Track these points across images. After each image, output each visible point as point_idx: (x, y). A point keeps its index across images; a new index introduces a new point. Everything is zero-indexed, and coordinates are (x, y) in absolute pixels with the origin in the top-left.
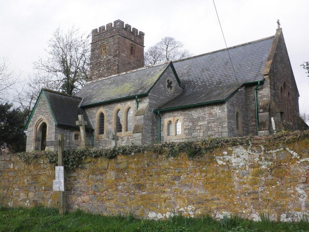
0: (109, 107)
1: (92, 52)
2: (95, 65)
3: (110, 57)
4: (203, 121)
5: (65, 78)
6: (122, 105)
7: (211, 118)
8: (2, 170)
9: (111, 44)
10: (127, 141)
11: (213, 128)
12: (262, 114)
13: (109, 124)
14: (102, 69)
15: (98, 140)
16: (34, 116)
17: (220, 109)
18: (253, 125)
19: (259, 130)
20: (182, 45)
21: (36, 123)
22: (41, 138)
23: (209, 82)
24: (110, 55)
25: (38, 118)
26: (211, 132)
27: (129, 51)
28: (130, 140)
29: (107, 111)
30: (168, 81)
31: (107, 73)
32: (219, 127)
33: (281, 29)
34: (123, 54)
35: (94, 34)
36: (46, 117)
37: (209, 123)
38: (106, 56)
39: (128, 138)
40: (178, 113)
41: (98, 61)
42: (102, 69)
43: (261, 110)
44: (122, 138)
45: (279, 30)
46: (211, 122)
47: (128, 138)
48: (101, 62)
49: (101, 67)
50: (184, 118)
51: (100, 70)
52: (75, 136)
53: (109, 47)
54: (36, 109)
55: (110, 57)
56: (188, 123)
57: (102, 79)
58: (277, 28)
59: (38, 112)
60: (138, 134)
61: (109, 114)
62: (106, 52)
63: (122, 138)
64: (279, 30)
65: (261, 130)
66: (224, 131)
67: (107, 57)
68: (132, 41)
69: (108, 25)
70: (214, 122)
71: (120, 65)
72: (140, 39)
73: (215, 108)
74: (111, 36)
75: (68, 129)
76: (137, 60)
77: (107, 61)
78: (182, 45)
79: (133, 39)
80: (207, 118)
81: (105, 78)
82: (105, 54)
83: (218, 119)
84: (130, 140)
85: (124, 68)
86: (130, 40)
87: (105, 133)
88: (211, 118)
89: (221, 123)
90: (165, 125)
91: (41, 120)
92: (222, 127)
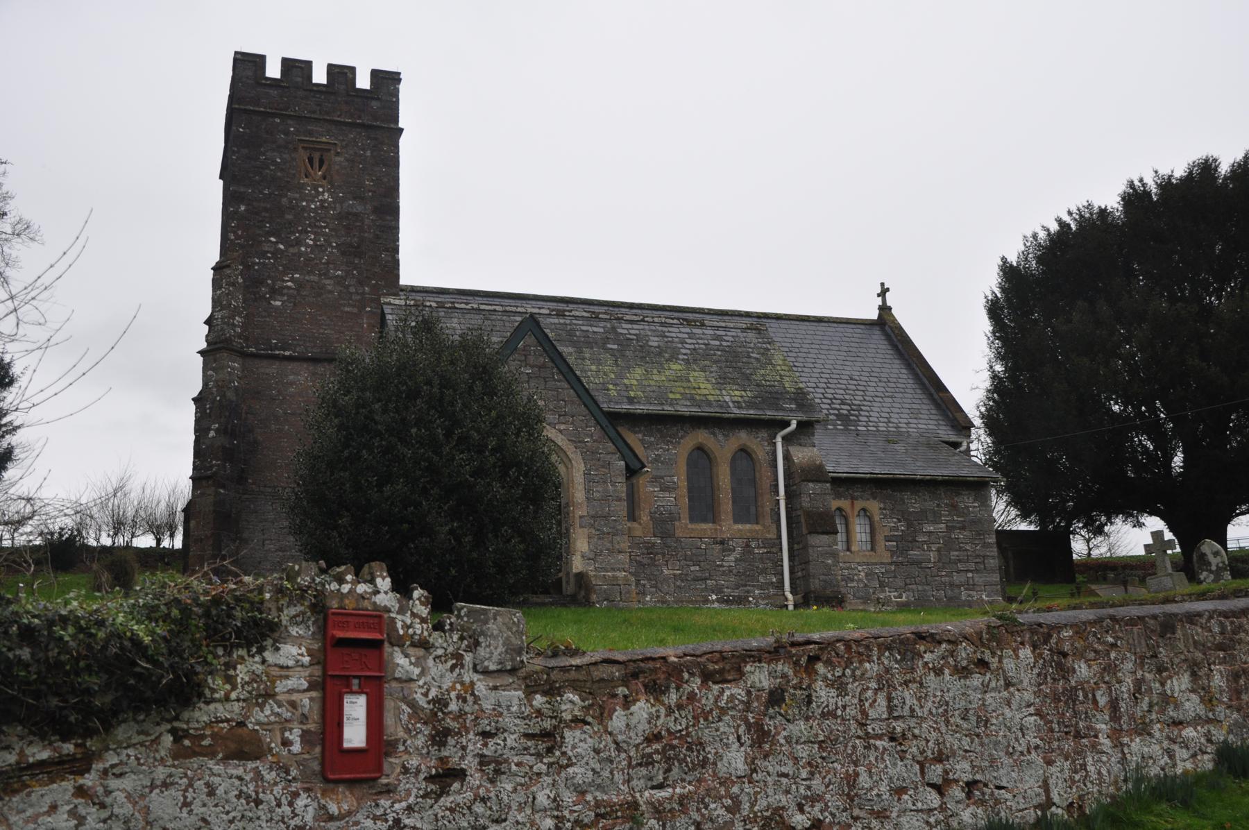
6: (714, 434)
10: (743, 554)
17: (975, 501)
29: (651, 443)
36: (561, 431)
37: (950, 529)
39: (748, 546)
41: (284, 200)
44: (722, 543)
47: (748, 546)
51: (299, 243)
63: (722, 543)
70: (963, 528)
77: (340, 217)
83: (973, 522)
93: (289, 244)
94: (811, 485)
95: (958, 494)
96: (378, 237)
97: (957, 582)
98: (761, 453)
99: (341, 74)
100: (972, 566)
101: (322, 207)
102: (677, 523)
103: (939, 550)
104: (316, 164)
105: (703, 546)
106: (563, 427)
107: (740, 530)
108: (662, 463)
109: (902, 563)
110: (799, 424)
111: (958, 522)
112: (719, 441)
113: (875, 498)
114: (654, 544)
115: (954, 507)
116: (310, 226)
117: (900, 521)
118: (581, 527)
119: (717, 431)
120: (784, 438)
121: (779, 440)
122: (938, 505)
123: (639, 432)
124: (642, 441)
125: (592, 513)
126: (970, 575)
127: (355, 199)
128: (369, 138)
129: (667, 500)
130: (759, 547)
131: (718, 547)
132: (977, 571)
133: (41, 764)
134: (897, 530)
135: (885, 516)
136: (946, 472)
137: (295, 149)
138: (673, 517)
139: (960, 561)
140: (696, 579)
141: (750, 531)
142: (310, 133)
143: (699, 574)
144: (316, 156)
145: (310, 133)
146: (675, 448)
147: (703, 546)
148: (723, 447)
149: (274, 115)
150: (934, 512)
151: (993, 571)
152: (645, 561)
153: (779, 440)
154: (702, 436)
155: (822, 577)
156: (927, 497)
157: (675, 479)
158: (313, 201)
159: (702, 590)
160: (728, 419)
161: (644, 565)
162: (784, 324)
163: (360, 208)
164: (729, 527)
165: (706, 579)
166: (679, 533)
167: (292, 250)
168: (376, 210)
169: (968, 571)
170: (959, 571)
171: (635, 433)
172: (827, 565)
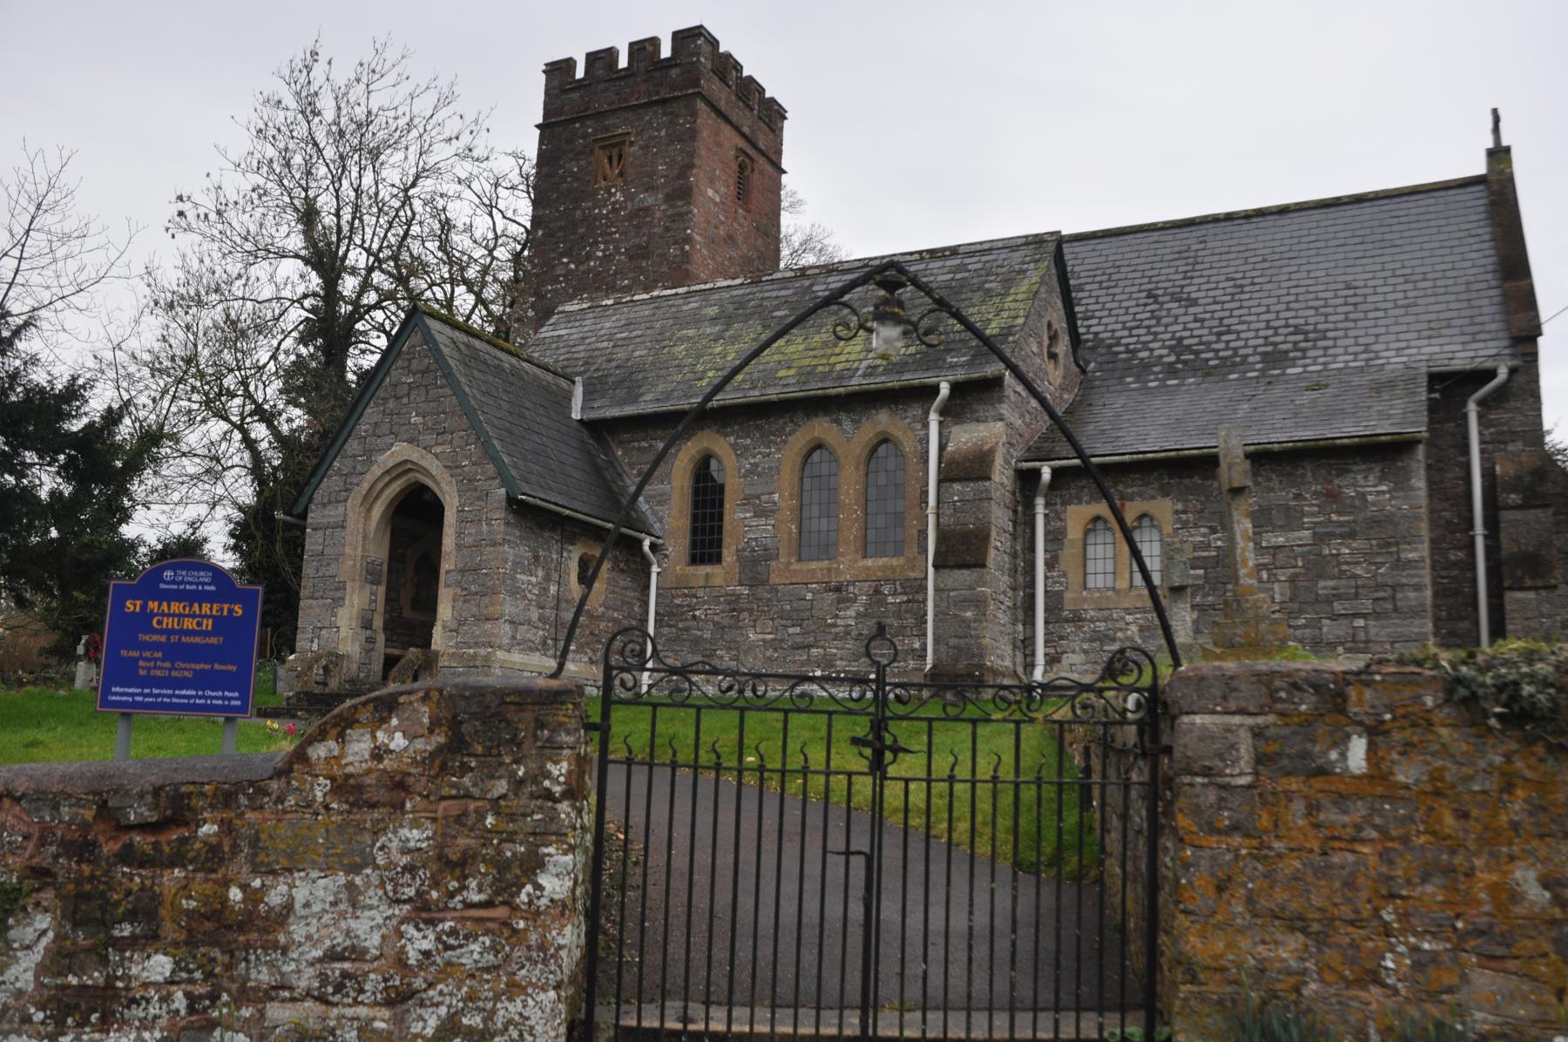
0: (758, 428)
1: (545, 170)
2: (561, 229)
3: (648, 199)
4: (1287, 528)
5: (315, 295)
6: (838, 422)
7: (1334, 517)
8: (1243, 781)
9: (651, 138)
10: (867, 606)
11: (1347, 563)
12: (1518, 515)
13: (756, 515)
14: (603, 251)
15: (685, 595)
16: (353, 446)
17: (1381, 480)
18: (1455, 564)
19: (1511, 589)
20: (800, 202)
21: (366, 486)
22: (385, 567)
23: (1152, 350)
24: (650, 188)
25: (386, 460)
26: (1331, 583)
27: (731, 182)
28: (890, 599)
29: (746, 448)
30: (1050, 325)
31: (631, 275)
32: (1379, 560)
33: (1508, 150)
34: (710, 192)
35: (556, 83)
36: (436, 455)
37: (1320, 538)
38: (623, 191)
39: (877, 591)
40: (1147, 484)
41: (578, 213)
42: (603, 251)
43: (1514, 498)
44: (838, 589)
45: (1499, 155)
46: (1332, 535)
47: (877, 591)
48: (595, 218)
49: (597, 243)
50: (1179, 506)
51: (589, 257)
52: (581, 560)
53: (646, 148)
54: (369, 411)
55: (648, 199)
56: (1204, 535)
57: (655, 293)
58: (1491, 145)
59: (385, 428)
60: (966, 572)
61: (756, 465)
62: (621, 174)
63: (838, 589)
64: (1499, 155)
65: (1522, 589)
66: (1405, 581)
67: (629, 197)
68: (743, 135)
69: (637, 48)
70: (1352, 535)
71: (698, 238)
72: (771, 136)
73: (1355, 468)
74: (657, 102)
75: (553, 530)
76: (757, 229)
77: (631, 216)
78: (800, 202)
79: (746, 130)
80: (1313, 514)
81: (673, 291)
82: (620, 182)
83: (1375, 522)
84: (890, 599)
85: (713, 259)
86: (738, 129)
87: (728, 555)
88: (1334, 517)
89: (1389, 545)
90: (1069, 537)
91: (404, 467)
92: (1399, 565)
93: (579, 263)
94: (957, 486)
95: (1343, 472)
96: (667, 229)
97: (1331, 638)
98: (909, 445)
99: (644, 49)
100: (1367, 605)
101: (614, 209)
102: (773, 563)
103: (1292, 580)
104: (615, 162)
105: (809, 596)
106: (439, 449)
107: (868, 568)
108: (759, 475)
109: (1212, 607)
110: (956, 387)
111: (1340, 524)
112: (845, 432)
113: (1166, 495)
114: (739, 596)
115: (1332, 496)
116: (601, 235)
117: (1213, 530)
118: (447, 586)
119: (843, 416)
120: (1480, 403)
121: (1472, 410)
122: (1298, 497)
123: (732, 433)
124: (734, 446)
125: (460, 565)
126: (1360, 622)
127: (646, 191)
128: (664, 114)
129: (763, 530)
130: (894, 594)
131: (832, 596)
132: (1376, 615)
133: (1156, 806)
134: (1207, 547)
135: (1185, 525)
136: (1354, 431)
137: (592, 152)
138: (769, 555)
139: (1339, 597)
140: (797, 647)
141: (884, 568)
142: (607, 129)
143: (799, 639)
144: (615, 152)
145: (607, 129)
146: (779, 450)
147: (809, 596)
148: (848, 438)
149: (574, 120)
150: (1288, 508)
151: (1416, 613)
152: (725, 622)
153: (1472, 410)
154: (821, 427)
155: (953, 641)
156: (1275, 483)
157: (776, 497)
158: (605, 206)
159: (803, 664)
160: (838, 396)
161: (723, 628)
162: (1199, 232)
163: (650, 201)
164: (850, 565)
165: (810, 646)
166: (774, 579)
167: (582, 268)
168: (669, 198)
169: (1356, 616)
170: (1335, 617)
171: (726, 435)
172: (964, 620)
